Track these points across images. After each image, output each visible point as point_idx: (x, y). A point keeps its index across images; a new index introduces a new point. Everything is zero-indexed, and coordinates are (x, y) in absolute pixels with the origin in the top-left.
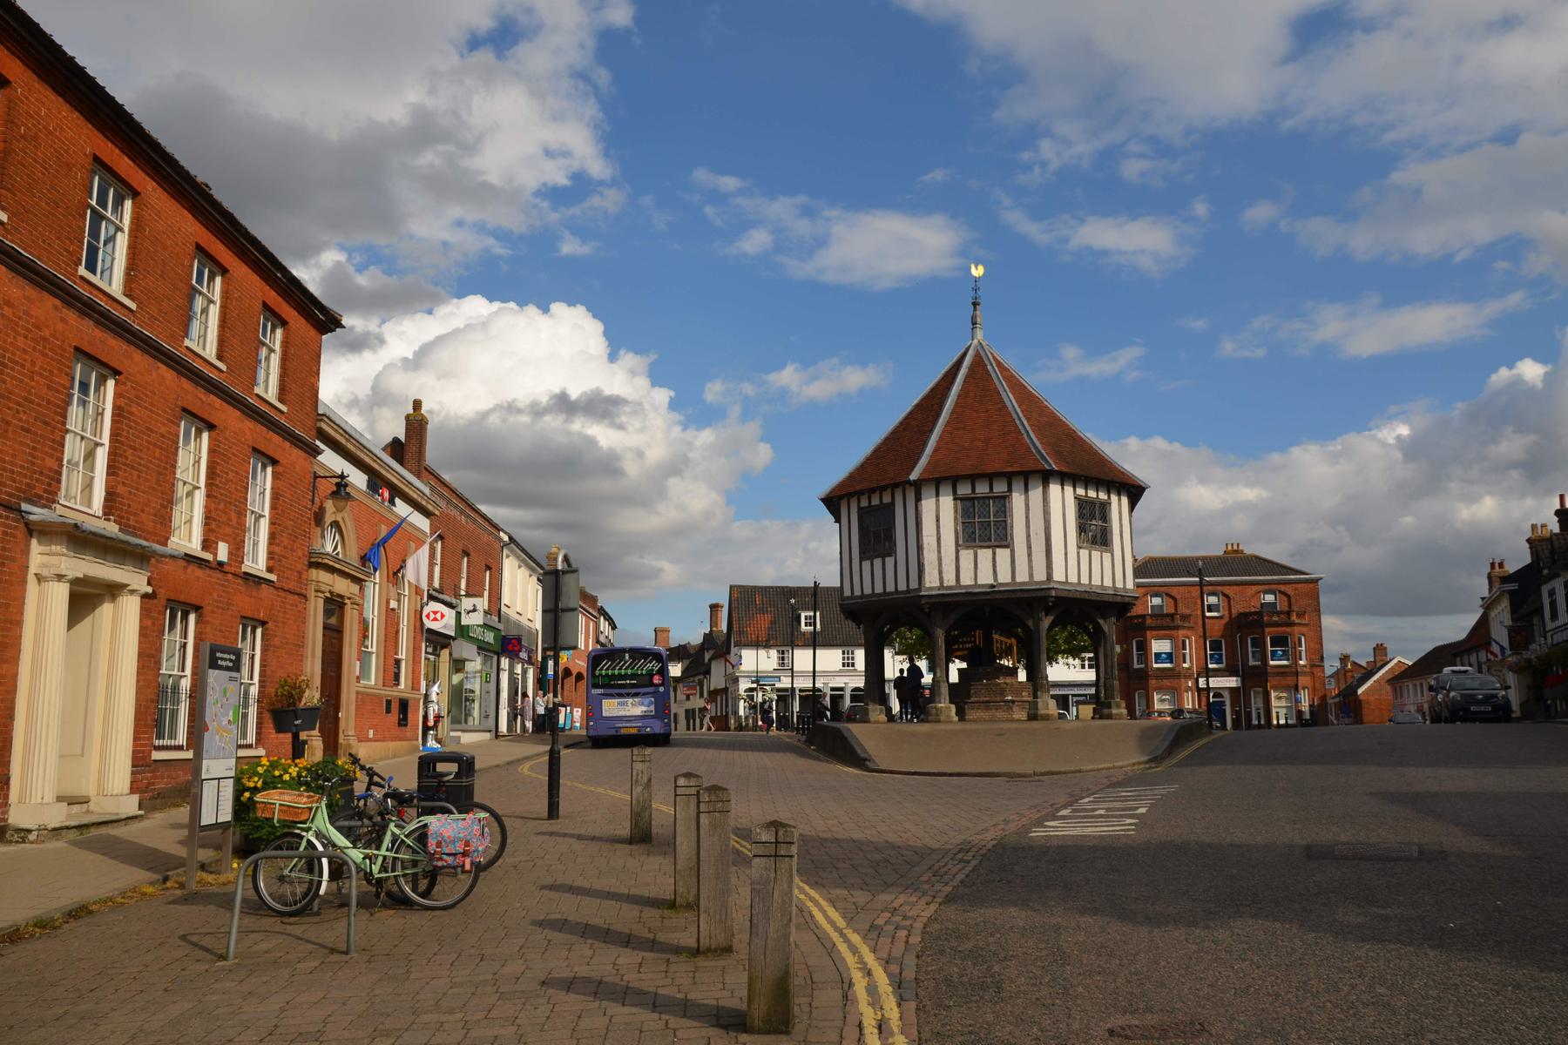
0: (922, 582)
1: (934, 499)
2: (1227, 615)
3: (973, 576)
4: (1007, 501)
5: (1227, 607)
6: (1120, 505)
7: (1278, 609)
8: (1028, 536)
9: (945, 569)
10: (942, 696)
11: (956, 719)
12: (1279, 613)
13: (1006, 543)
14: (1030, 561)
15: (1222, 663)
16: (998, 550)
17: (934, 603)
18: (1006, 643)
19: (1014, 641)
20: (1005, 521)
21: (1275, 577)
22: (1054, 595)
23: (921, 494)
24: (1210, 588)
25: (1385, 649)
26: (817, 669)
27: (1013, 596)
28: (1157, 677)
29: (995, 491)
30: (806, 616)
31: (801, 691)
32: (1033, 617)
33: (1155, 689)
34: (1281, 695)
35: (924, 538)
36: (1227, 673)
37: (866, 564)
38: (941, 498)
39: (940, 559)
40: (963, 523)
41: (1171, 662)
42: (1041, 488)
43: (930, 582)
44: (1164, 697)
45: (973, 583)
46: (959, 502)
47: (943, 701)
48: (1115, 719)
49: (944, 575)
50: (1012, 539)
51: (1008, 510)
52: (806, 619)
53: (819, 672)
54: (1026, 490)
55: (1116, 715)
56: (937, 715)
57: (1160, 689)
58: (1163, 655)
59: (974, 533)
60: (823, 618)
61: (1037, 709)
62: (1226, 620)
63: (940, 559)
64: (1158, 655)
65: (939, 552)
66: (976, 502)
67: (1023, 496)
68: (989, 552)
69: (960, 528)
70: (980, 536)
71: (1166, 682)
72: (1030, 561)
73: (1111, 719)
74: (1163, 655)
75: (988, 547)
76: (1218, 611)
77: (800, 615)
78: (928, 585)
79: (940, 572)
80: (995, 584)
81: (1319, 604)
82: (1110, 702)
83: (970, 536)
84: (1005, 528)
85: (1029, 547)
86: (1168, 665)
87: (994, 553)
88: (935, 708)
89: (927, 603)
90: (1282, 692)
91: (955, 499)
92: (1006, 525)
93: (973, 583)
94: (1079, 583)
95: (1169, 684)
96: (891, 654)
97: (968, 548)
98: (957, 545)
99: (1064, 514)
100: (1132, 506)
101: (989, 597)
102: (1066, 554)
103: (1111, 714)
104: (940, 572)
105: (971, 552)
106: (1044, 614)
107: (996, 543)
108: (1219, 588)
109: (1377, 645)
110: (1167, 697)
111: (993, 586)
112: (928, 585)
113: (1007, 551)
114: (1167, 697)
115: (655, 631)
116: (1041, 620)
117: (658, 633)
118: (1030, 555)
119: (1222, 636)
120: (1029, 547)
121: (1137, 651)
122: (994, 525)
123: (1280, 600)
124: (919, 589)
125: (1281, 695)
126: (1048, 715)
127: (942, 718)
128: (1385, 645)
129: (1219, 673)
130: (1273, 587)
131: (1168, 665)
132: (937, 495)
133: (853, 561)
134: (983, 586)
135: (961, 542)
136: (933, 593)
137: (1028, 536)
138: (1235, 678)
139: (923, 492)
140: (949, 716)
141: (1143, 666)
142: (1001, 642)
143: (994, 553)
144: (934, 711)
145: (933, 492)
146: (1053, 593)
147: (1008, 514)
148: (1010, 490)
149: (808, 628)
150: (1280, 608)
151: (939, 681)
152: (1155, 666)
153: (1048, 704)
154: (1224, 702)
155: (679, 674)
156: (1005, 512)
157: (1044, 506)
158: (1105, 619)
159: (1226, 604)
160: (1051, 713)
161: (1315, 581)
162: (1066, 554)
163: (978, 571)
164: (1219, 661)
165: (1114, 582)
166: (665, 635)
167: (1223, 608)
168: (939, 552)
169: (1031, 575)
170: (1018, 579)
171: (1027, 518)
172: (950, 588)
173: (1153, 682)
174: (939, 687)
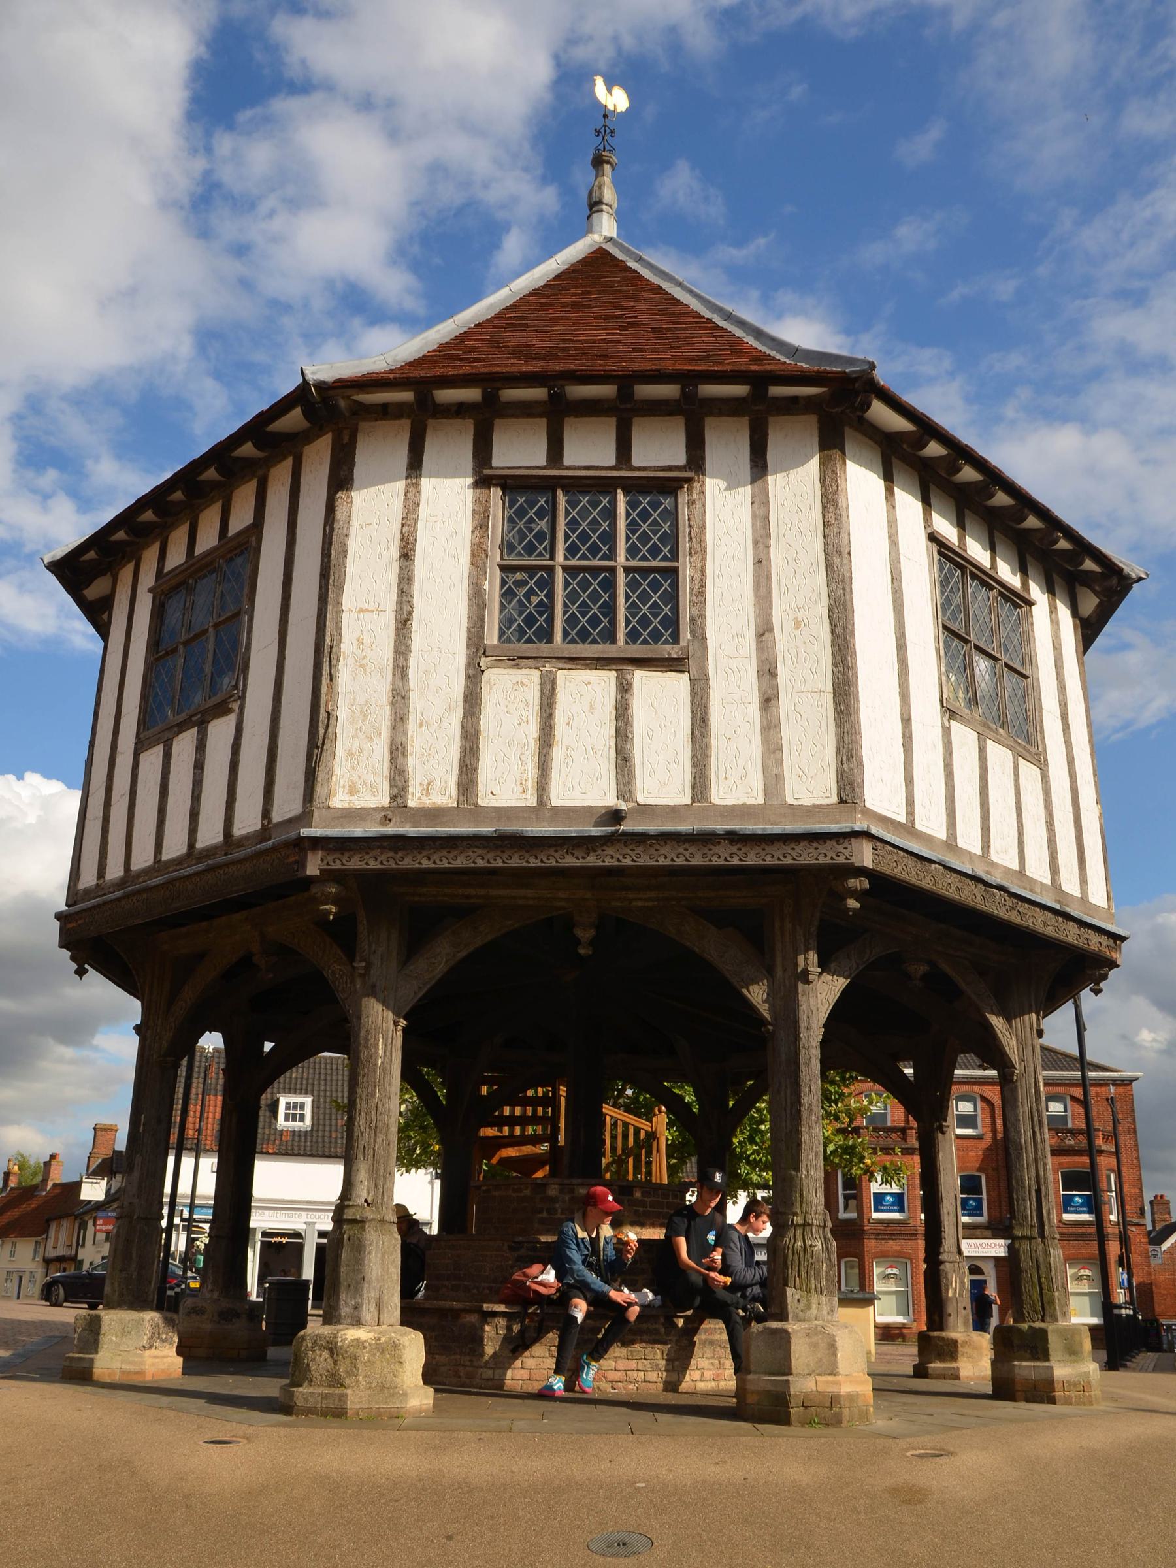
0: (320, 790)
1: (400, 486)
2: (989, 1134)
3: (532, 773)
4: (683, 498)
5: (988, 1121)
6: (1055, 623)
7: (1070, 1125)
8: (764, 630)
9: (417, 737)
10: (369, 1293)
11: (421, 1398)
12: (1073, 1132)
13: (673, 651)
14: (770, 727)
15: (981, 1215)
16: (641, 678)
17: (361, 876)
18: (637, 1131)
19: (661, 1119)
20: (674, 572)
21: (1065, 1074)
22: (868, 863)
23: (352, 464)
24: (963, 1088)
25: (1168, 1203)
26: (198, 1192)
27: (698, 861)
28: (1090, 1235)
29: (636, 462)
30: (288, 1103)
31: (265, 1234)
32: (770, 972)
33: (876, 1256)
34: (1082, 1272)
35: (346, 618)
36: (989, 1233)
37: (152, 759)
38: (426, 483)
39: (399, 698)
40: (504, 569)
41: (901, 1210)
42: (813, 466)
43: (353, 790)
44: (889, 1271)
45: (532, 801)
46: (496, 493)
47: (368, 1313)
48: (1068, 1402)
49: (412, 763)
50: (700, 636)
51: (683, 529)
52: (287, 1108)
53: (261, 1200)
54: (759, 467)
55: (1068, 1385)
56: (335, 1380)
57: (882, 1256)
58: (888, 1198)
59: (547, 608)
60: (318, 1107)
61: (784, 1367)
62: (987, 1142)
63: (399, 698)
64: (879, 1198)
65: (401, 670)
66: (561, 498)
67: (746, 492)
68: (604, 682)
69: (492, 586)
70: (571, 621)
71: (893, 1245)
72: (770, 727)
73: (1052, 1401)
74: (888, 1198)
75: (602, 663)
76: (975, 1126)
77: (278, 1100)
78: (340, 800)
79: (397, 751)
80: (623, 806)
81: (1134, 1120)
82: (1044, 1332)
83: (530, 621)
84: (673, 597)
85: (768, 671)
86: (896, 1216)
87: (624, 689)
88: (332, 1348)
89: (328, 875)
90: (1083, 1268)
91: (483, 482)
92: (675, 585)
93: (532, 801)
94: (951, 844)
95: (898, 1248)
96: (428, 1177)
97: (518, 660)
98: (476, 647)
99: (896, 578)
100: (1089, 631)
101: (592, 861)
102: (906, 721)
103: (1049, 1383)
104: (397, 751)
105: (530, 678)
106: (813, 956)
107: (637, 650)
108: (976, 1088)
109: (1156, 1197)
110: (895, 1271)
111: (615, 816)
112: (340, 800)
113: (677, 685)
114: (895, 1271)
115: (95, 1129)
116: (804, 977)
117: (99, 1133)
118: (768, 700)
119: (980, 1169)
120: (768, 671)
121: (845, 1189)
122: (632, 585)
123: (1073, 1111)
124: (305, 817)
125: (1082, 1272)
126: (834, 1400)
127: (356, 1398)
128: (1166, 1198)
129: (978, 1232)
130: (1062, 1090)
131: (896, 1216)
132: (415, 466)
133: (105, 778)
134: (569, 813)
135: (492, 637)
136: (358, 831)
137: (764, 630)
138: (1002, 1242)
139: (359, 458)
140: (387, 1388)
141: (854, 1215)
142: (626, 1125)
143: (624, 689)
144: (319, 1362)
145: (401, 457)
146: (866, 856)
147: (684, 545)
148: (696, 462)
149: (290, 1124)
150: (1074, 1123)
151: (360, 1223)
152: (875, 1215)
153: (832, 1347)
154: (985, 1282)
155: (100, 1197)
156: (672, 539)
157: (826, 524)
158: (1009, 1019)
159: (988, 1115)
160: (846, 1389)
161: (1126, 1083)
162: (906, 721)
163: (557, 753)
164: (976, 1211)
165: (1054, 871)
166: (109, 1136)
167: (983, 1121)
168: (401, 670)
169: (773, 781)
170: (723, 794)
171: (761, 563)
172: (434, 814)
173: (870, 1245)
174: (359, 1248)
